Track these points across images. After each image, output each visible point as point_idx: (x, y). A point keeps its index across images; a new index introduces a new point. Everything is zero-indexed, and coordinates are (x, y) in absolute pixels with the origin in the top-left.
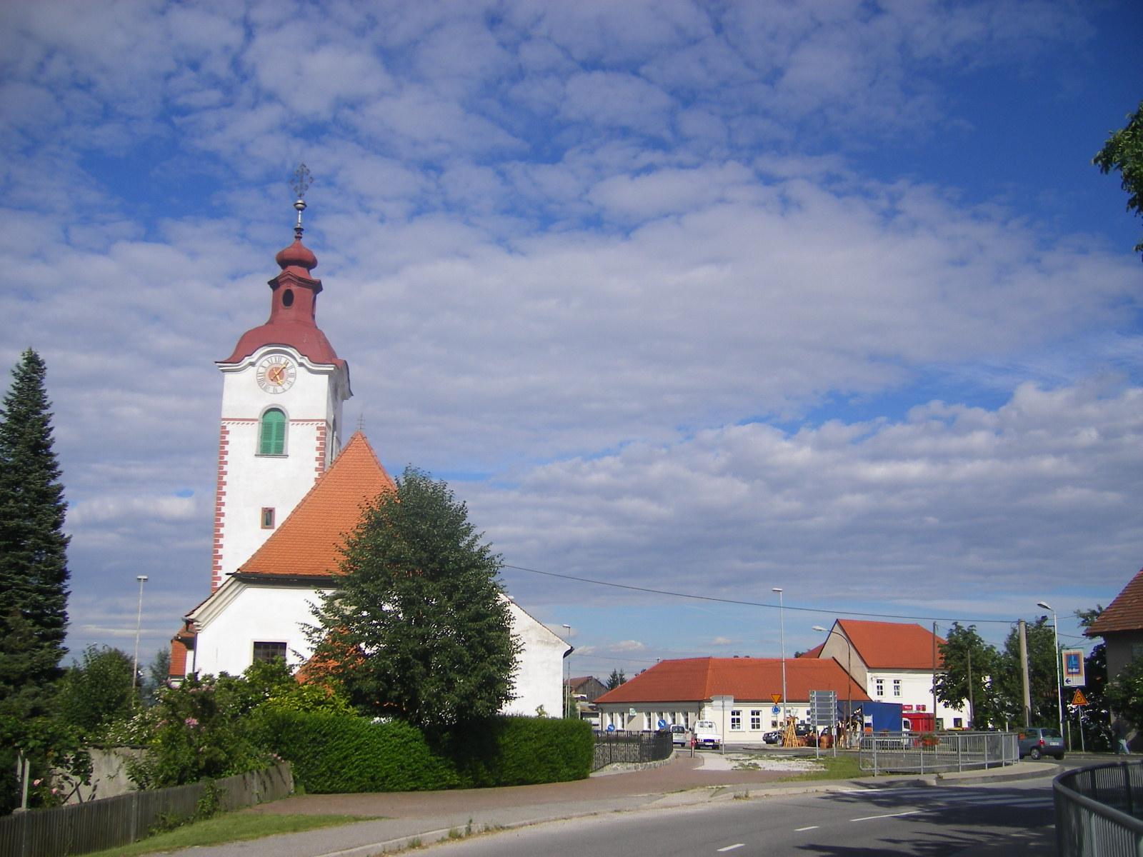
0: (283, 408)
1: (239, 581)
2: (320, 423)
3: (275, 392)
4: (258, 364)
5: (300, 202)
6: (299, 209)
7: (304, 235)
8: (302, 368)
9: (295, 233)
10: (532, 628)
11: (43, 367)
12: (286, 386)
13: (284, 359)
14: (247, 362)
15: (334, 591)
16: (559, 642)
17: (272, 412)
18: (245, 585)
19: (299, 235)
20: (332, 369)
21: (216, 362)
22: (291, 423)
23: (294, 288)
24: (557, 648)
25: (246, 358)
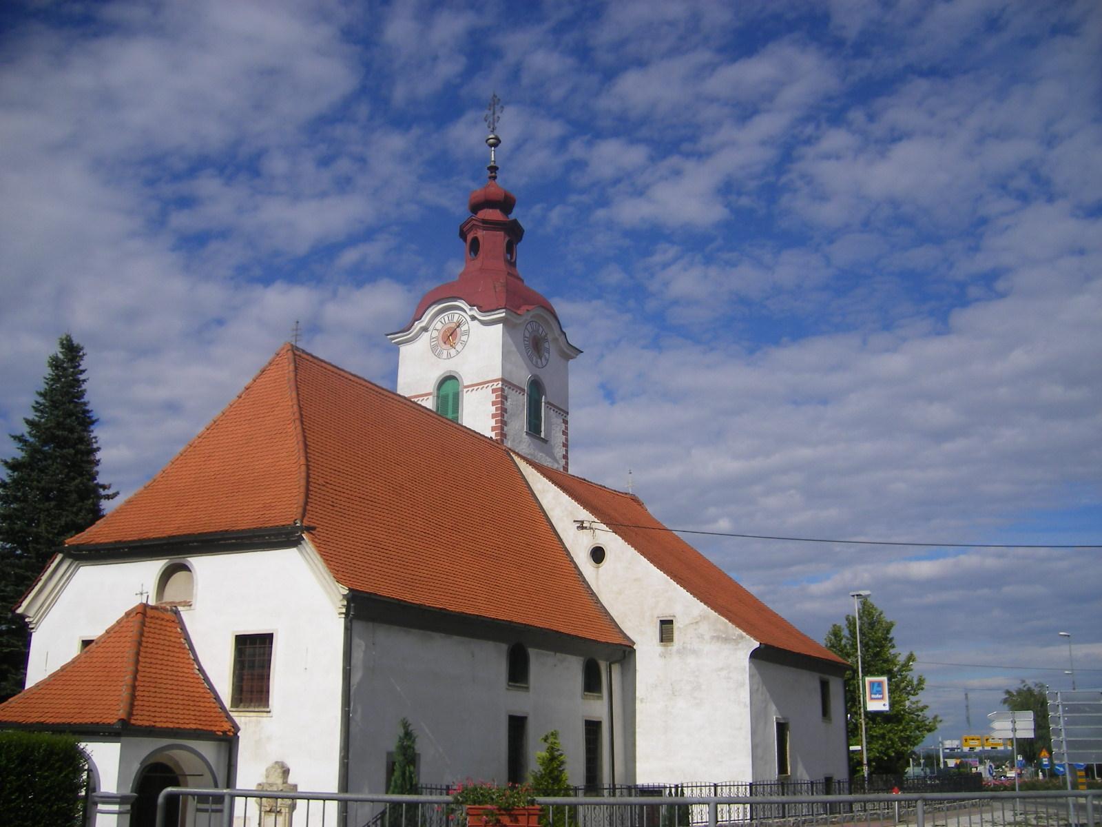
0: (457, 373)
1: (70, 557)
2: (496, 384)
3: (449, 357)
4: (431, 328)
5: (491, 136)
6: (491, 145)
7: (498, 174)
8: (476, 322)
9: (488, 173)
10: (704, 617)
11: (81, 354)
12: (459, 347)
13: (456, 316)
14: (418, 328)
15: (167, 560)
16: (742, 637)
17: (448, 382)
18: (77, 562)
19: (493, 174)
20: (504, 314)
21: (388, 335)
22: (465, 390)
23: (480, 234)
24: (740, 645)
25: (416, 323)
